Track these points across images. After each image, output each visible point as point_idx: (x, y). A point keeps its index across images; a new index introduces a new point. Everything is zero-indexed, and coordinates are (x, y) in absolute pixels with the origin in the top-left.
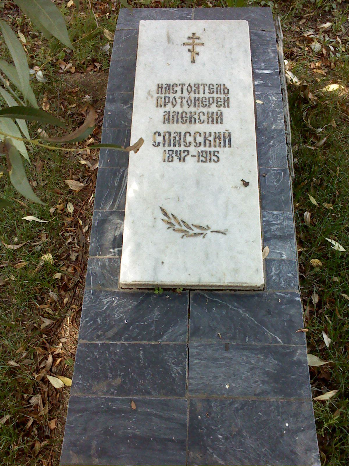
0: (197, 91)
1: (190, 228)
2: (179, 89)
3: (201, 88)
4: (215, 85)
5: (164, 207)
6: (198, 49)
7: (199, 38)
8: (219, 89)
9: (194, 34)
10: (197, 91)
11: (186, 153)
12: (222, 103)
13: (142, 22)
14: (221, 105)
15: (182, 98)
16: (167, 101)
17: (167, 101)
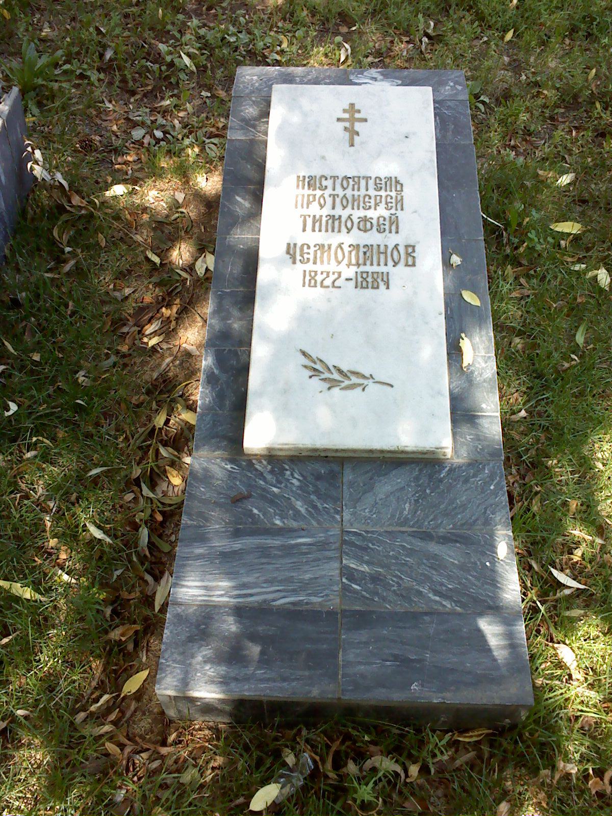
0: (356, 187)
1: (346, 376)
2: (329, 183)
3: (363, 183)
4: (383, 179)
5: (303, 349)
6: (358, 126)
7: (359, 111)
8: (388, 183)
9: (352, 105)
10: (356, 187)
11: (325, 275)
12: (394, 205)
13: (430, 89)
14: (392, 207)
15: (334, 196)
16: (378, 201)
17: (378, 201)
